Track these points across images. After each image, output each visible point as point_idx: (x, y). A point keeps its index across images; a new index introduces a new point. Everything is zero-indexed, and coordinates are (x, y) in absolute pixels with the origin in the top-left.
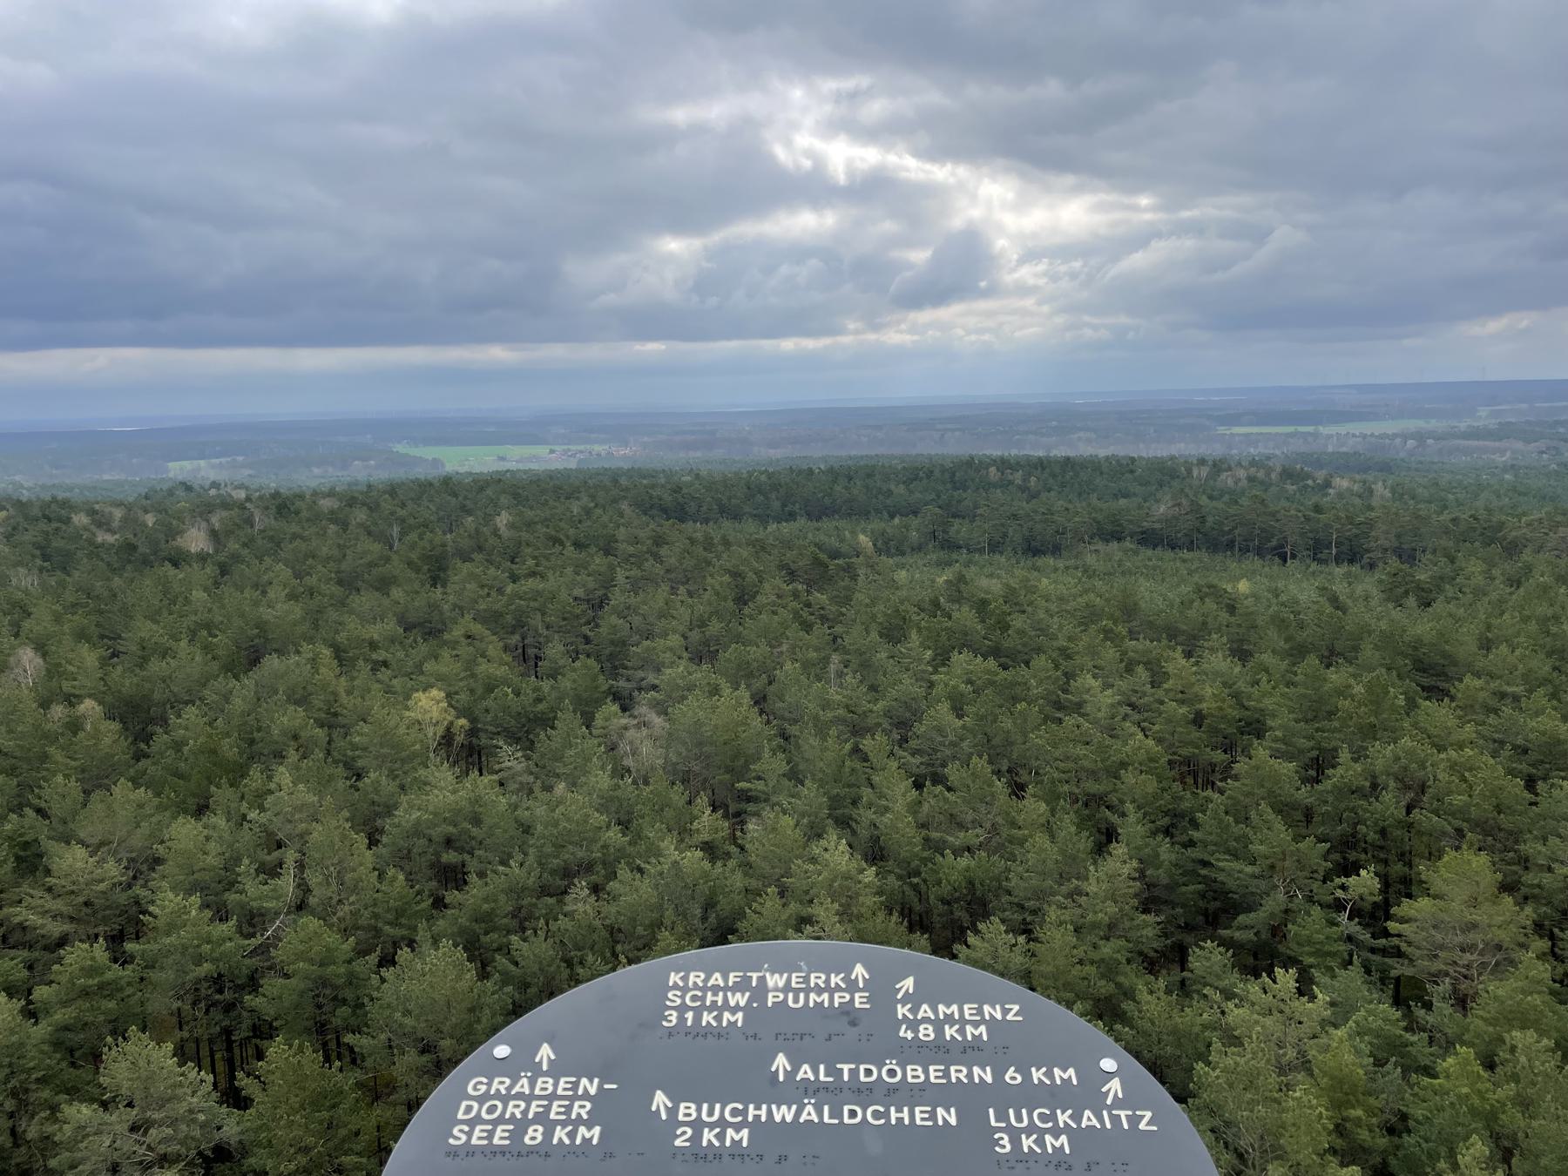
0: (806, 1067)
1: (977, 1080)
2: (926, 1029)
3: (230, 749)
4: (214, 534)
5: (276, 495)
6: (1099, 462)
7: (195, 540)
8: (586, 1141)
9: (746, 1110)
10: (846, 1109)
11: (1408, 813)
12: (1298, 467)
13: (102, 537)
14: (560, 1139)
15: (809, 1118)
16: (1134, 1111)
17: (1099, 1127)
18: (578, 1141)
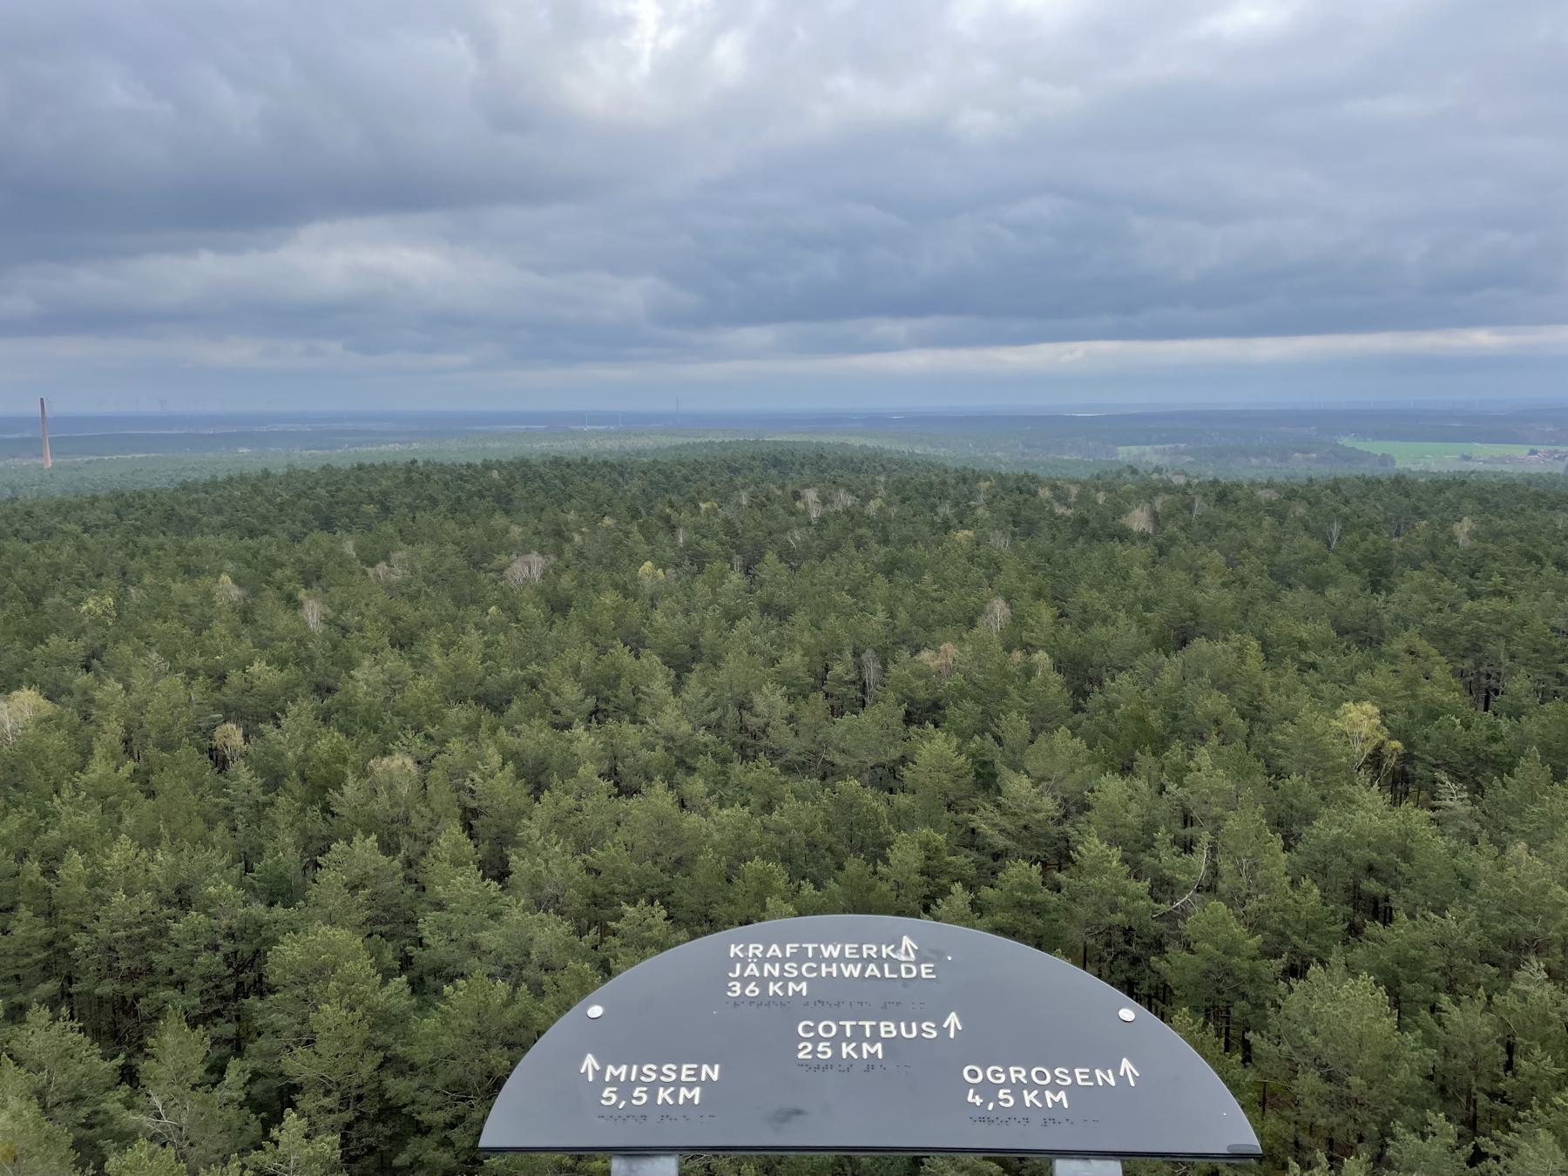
4: (1155, 517)
7: (1138, 520)
13: (1060, 510)
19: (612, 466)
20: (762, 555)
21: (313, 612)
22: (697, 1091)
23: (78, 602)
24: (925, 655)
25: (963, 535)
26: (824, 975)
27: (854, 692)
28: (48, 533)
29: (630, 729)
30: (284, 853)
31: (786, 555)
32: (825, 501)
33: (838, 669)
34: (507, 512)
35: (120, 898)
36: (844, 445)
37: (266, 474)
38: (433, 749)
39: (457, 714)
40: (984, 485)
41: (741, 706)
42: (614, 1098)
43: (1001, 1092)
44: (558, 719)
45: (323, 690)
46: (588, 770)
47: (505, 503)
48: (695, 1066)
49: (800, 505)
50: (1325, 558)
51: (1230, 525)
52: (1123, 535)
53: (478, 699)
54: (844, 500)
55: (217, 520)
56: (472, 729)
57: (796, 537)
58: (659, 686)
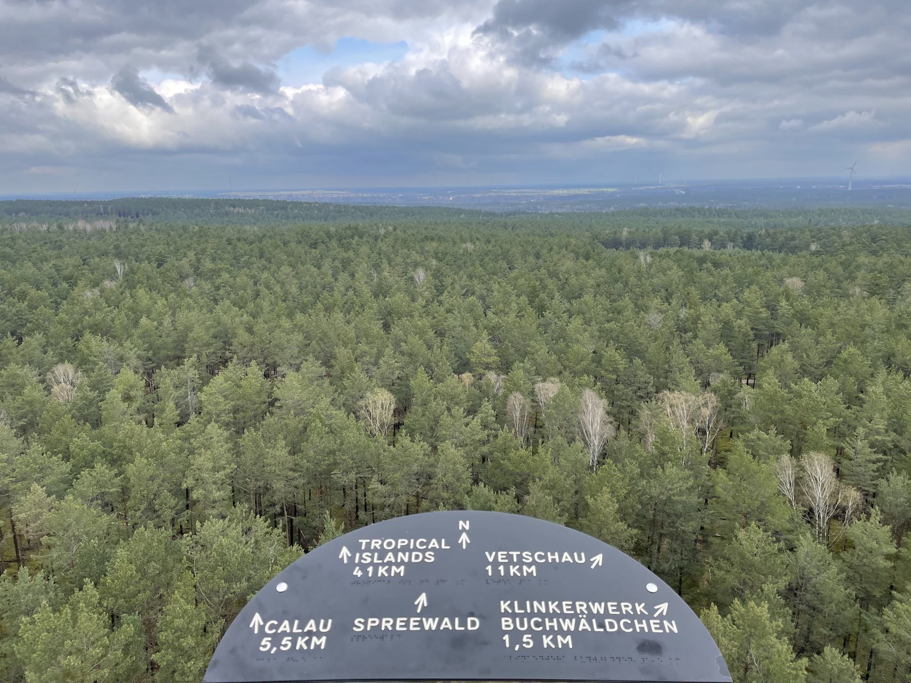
0: (434, 541)
1: (543, 603)
2: (506, 621)
3: (413, 500)
8: (317, 647)
9: (544, 622)
10: (469, 619)
14: (301, 646)
15: (446, 626)
16: (276, 632)
17: (590, 630)
18: (312, 647)
22: (402, 568)
26: (550, 561)
42: (269, 645)
43: (525, 636)
48: (405, 619)
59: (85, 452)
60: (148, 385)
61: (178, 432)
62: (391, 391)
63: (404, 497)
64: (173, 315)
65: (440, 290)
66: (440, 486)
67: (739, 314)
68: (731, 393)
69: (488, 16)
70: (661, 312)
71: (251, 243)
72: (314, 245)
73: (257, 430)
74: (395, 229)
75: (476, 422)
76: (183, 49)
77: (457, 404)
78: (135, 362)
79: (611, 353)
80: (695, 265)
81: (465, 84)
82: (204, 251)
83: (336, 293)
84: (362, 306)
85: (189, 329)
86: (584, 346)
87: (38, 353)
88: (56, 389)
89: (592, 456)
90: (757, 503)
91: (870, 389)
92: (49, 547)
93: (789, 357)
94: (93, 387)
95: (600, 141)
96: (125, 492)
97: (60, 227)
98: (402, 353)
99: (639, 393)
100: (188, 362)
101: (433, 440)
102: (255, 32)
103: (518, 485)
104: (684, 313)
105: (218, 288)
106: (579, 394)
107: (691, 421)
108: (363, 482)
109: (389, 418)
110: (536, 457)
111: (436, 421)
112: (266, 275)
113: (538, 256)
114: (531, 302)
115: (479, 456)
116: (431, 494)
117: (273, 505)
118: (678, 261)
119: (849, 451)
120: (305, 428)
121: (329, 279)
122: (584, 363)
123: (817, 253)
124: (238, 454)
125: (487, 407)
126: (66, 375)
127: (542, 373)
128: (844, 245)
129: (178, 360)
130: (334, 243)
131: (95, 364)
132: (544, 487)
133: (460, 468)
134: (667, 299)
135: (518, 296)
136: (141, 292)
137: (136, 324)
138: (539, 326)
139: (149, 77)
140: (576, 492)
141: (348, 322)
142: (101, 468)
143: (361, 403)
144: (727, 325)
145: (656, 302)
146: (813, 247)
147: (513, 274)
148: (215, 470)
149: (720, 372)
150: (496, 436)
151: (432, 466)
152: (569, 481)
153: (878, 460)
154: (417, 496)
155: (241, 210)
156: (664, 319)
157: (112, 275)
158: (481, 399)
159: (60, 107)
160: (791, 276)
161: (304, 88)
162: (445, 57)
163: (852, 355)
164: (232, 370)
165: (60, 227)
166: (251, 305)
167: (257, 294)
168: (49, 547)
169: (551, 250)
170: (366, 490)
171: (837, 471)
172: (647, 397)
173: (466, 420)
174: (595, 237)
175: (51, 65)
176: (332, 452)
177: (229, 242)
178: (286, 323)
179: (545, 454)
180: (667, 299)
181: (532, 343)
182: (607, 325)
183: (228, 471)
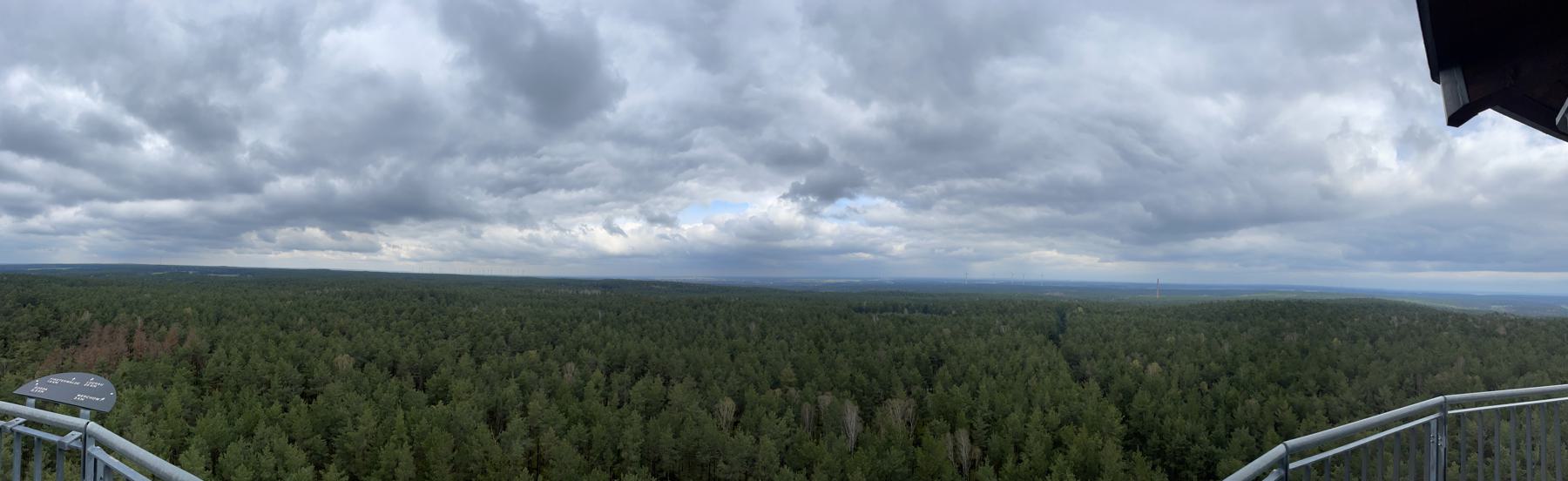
4: (1507, 329)
5: (1524, 319)
6: (1437, 315)
7: (1502, 330)
11: (424, 389)
12: (764, 429)
13: (1476, 326)
19: (1320, 305)
20: (1378, 338)
21: (1226, 347)
23: (1166, 338)
24: (1438, 376)
25: (1446, 333)
27: (1413, 389)
28: (1158, 316)
29: (1333, 399)
30: (1220, 430)
31: (1388, 339)
32: (1400, 321)
33: (1407, 380)
34: (1284, 318)
35: (1178, 435)
36: (1403, 302)
37: (1212, 303)
38: (1264, 399)
39: (1272, 387)
40: (1450, 317)
41: (1373, 393)
44: (1307, 393)
45: (1230, 374)
46: (1319, 412)
47: (1283, 314)
49: (1391, 322)
50: (1564, 346)
51: (1532, 333)
52: (1497, 335)
53: (1279, 383)
54: (1405, 321)
55: (1200, 316)
56: (1276, 393)
57: (1391, 332)
58: (1344, 383)
59: (575, 415)
60: (606, 380)
61: (617, 412)
62: (734, 400)
63: (738, 474)
64: (622, 342)
65: (764, 336)
66: (760, 467)
67: (923, 349)
68: (922, 397)
69: (787, 191)
70: (886, 350)
71: (663, 305)
72: (695, 307)
73: (657, 419)
74: (739, 299)
75: (783, 422)
76: (635, 208)
77: (772, 409)
78: (602, 366)
79: (861, 377)
80: (900, 322)
81: (776, 223)
82: (639, 308)
83: (705, 336)
84: (719, 344)
85: (628, 351)
86: (845, 373)
87: (561, 354)
88: (566, 375)
89: (850, 446)
90: (937, 467)
91: (980, 387)
92: (552, 467)
93: (947, 373)
94: (582, 378)
95: (844, 256)
96: (590, 443)
97: (577, 292)
98: (741, 375)
99: (876, 401)
100: (627, 370)
101: (756, 434)
102: (671, 198)
103: (807, 467)
104: (897, 350)
105: (644, 329)
106: (843, 403)
107: (903, 418)
108: (714, 462)
109: (731, 418)
110: (818, 447)
111: (759, 420)
112: (668, 323)
113: (819, 316)
114: (816, 344)
115: (784, 446)
116: (755, 473)
117: (662, 471)
118: (892, 320)
119: (975, 425)
120: (683, 421)
121: (702, 327)
122: (845, 383)
123: (955, 315)
124: (647, 433)
125: (790, 412)
126: (571, 368)
127: (821, 389)
128: (966, 311)
129: (621, 368)
130: (706, 307)
131: (584, 364)
132: (823, 468)
133: (773, 455)
134: (888, 342)
135: (808, 340)
136: (608, 328)
137: (605, 344)
138: (820, 359)
139: (619, 222)
140: (842, 471)
141: (711, 354)
142: (580, 425)
143: (716, 406)
144: (918, 357)
145: (882, 344)
146: (954, 312)
147: (806, 326)
148: (634, 441)
149: (916, 384)
150: (795, 432)
151: (756, 452)
152: (838, 463)
153: (987, 428)
154: (746, 474)
155: (658, 287)
156: (887, 354)
157: (596, 318)
158: (786, 406)
159: (581, 237)
160: (945, 328)
161: (696, 225)
162: (766, 210)
163: (973, 369)
164: (646, 379)
165: (577, 292)
166: (659, 340)
167: (663, 335)
168: (552, 467)
169: (826, 313)
170: (715, 467)
171: (971, 438)
172: (880, 403)
173: (777, 420)
174: (849, 306)
175: (580, 218)
176: (697, 439)
177: (652, 304)
178: (677, 352)
179: (824, 445)
180: (888, 342)
181: (816, 369)
182: (857, 358)
183: (640, 443)
